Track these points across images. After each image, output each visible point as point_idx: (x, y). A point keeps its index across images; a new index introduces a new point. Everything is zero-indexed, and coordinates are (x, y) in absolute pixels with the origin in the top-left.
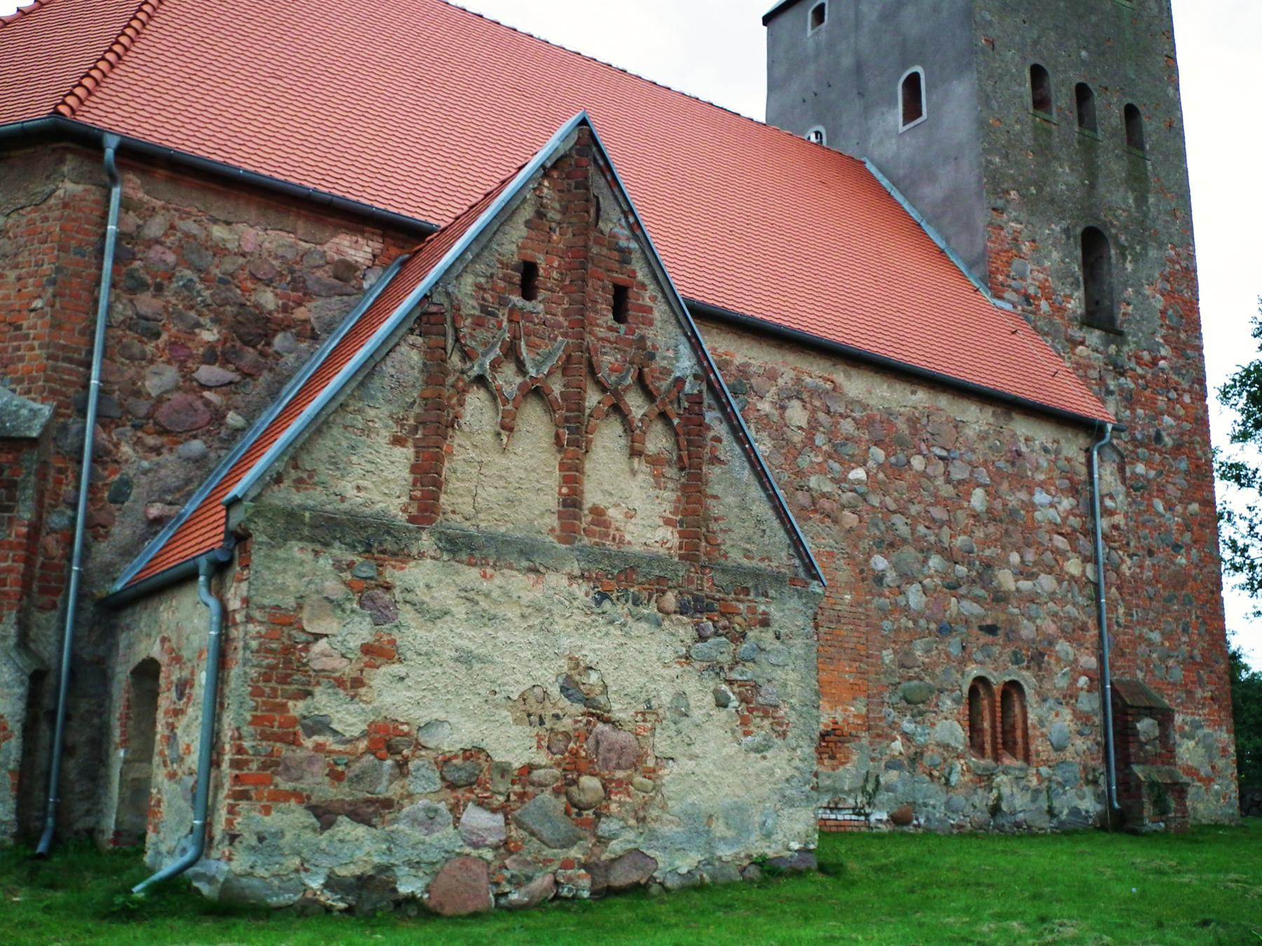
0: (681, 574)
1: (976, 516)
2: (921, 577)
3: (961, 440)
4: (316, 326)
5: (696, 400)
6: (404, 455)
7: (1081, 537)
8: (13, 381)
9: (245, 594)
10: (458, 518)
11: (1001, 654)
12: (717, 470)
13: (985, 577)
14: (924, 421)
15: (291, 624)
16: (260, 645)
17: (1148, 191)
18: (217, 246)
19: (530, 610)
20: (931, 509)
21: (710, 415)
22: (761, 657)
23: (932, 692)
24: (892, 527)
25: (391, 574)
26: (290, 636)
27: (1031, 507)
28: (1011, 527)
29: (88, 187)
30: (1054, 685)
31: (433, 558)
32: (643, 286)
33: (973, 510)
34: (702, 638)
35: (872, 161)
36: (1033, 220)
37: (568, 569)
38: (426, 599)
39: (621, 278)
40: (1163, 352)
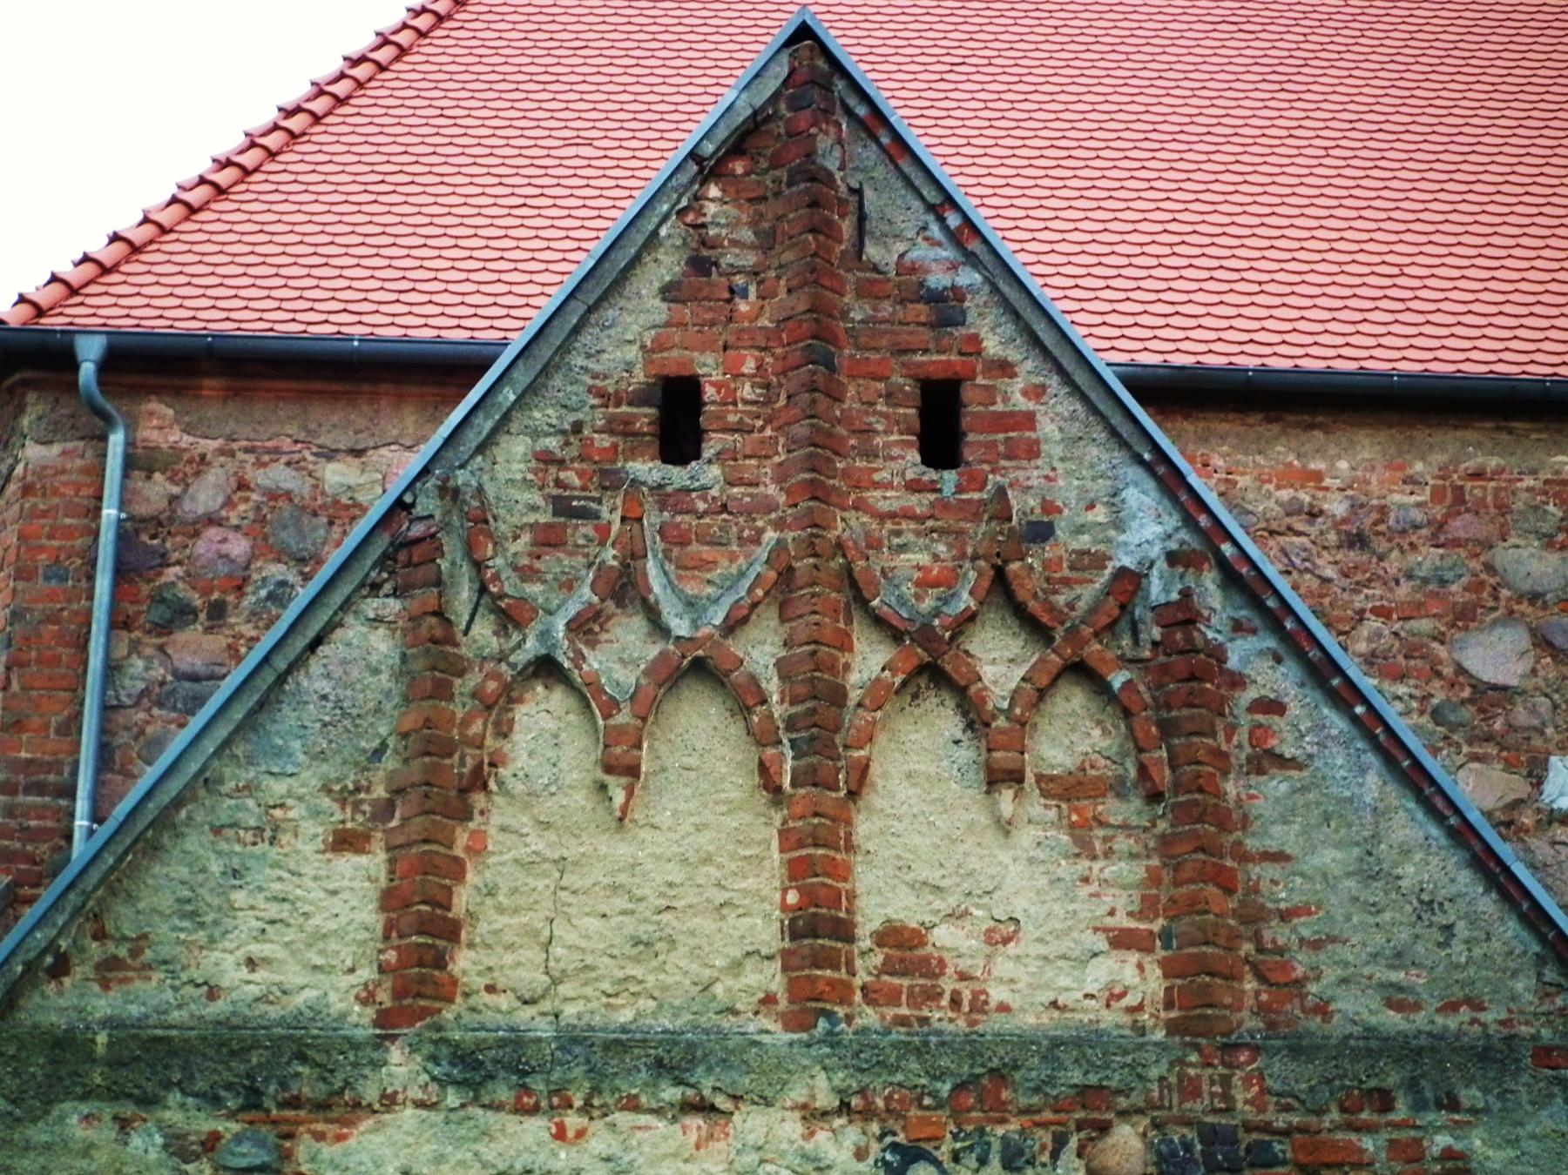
0: (1154, 1072)
5: (1183, 615)
10: (504, 1001)
12: (1277, 785)
18: (336, 502)
29: (70, 445)
31: (419, 1104)
32: (1005, 368)
37: (797, 1094)
39: (935, 361)
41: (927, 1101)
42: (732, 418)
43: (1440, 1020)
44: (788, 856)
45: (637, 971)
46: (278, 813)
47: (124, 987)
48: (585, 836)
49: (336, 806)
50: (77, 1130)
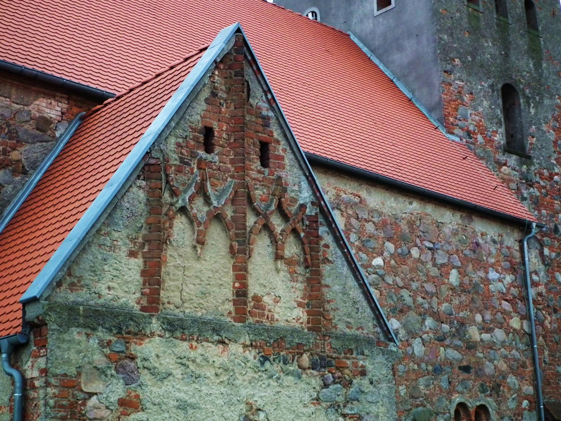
0: (311, 341)
1: (453, 289)
2: (421, 333)
3: (441, 235)
4: (26, 164)
6: (137, 263)
7: (519, 302)
9: (43, 366)
10: (172, 307)
11: (473, 386)
13: (461, 332)
14: (418, 223)
15: (74, 387)
16: (56, 402)
17: (541, 59)
19: (221, 370)
20: (425, 285)
21: (323, 230)
22: (362, 397)
23: (431, 415)
24: (401, 299)
25: (135, 348)
26: (73, 395)
27: (487, 281)
28: (475, 297)
30: (508, 407)
31: (160, 336)
32: (278, 142)
33: (451, 285)
34: (326, 386)
35: (355, 35)
36: (471, 79)
37: (242, 341)
38: (157, 365)
39: (264, 136)
40: (556, 171)
41: (268, 344)
42: (221, 143)
43: (356, 332)
44: (235, 273)
45: (202, 301)
46: (115, 242)
47: (77, 292)
48: (190, 261)
49: (130, 243)
50: (77, 337)
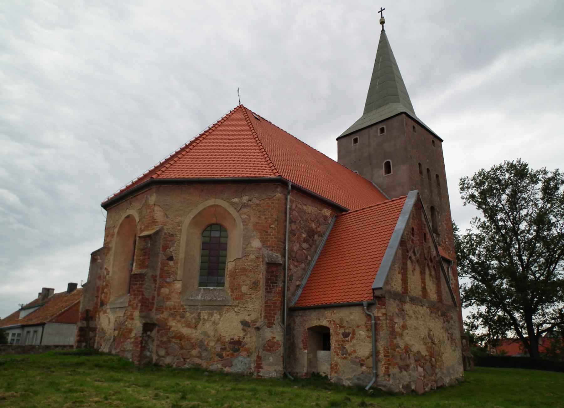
6: (400, 276)
8: (266, 247)
35: (375, 183)
